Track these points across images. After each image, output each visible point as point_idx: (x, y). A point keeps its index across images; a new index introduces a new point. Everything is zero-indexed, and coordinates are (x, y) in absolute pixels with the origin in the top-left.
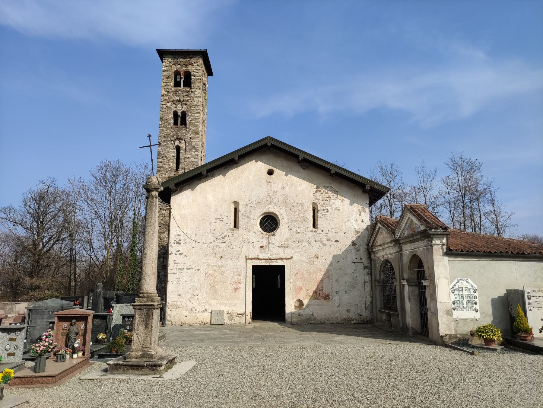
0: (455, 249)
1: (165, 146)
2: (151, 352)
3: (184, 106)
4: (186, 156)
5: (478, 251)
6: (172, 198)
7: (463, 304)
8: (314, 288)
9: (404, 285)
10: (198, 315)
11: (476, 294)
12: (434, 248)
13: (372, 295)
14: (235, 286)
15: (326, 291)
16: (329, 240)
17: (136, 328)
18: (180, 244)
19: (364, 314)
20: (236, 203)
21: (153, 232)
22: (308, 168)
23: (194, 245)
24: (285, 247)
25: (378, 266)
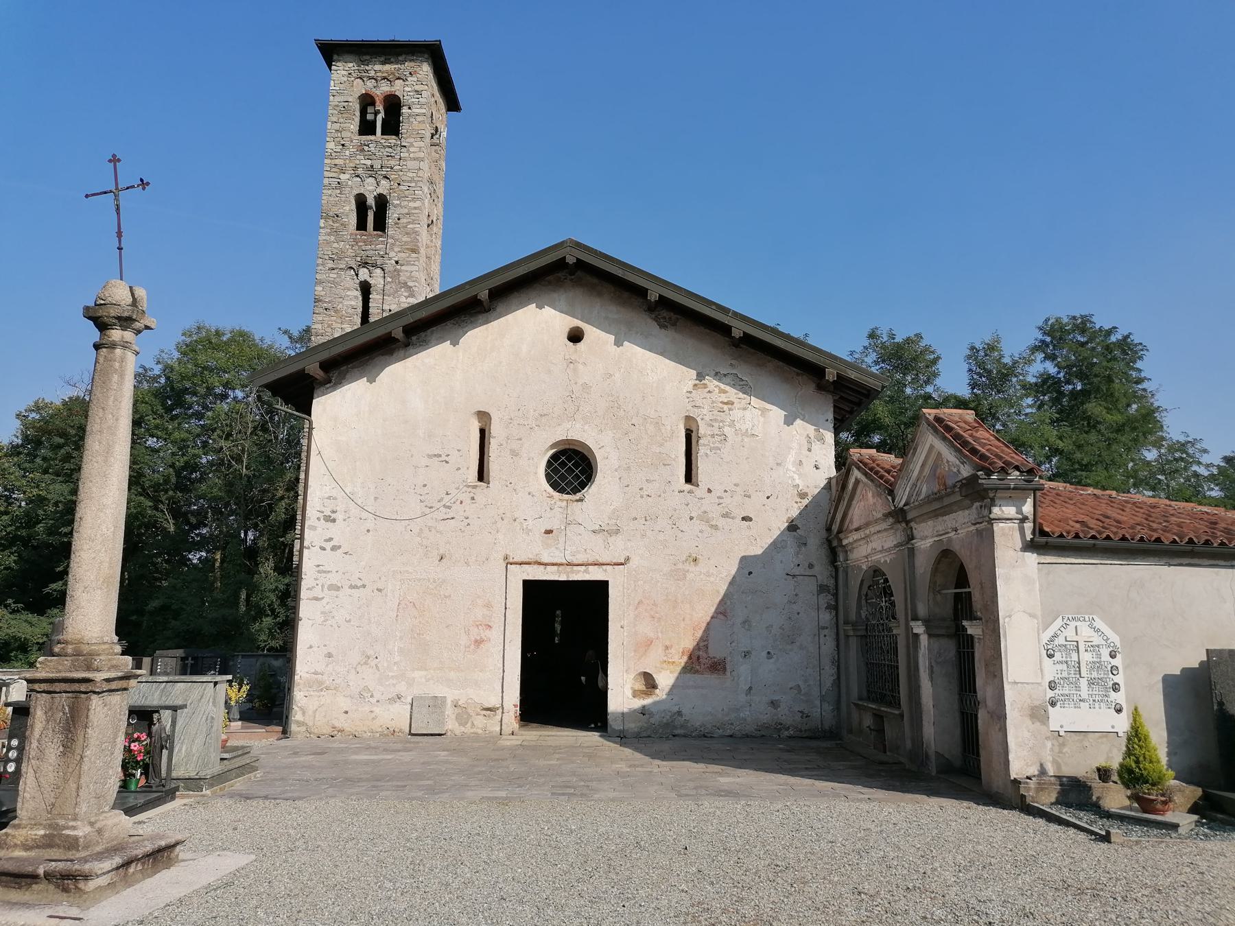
0: (1057, 532)
2: (74, 828)
3: (383, 182)
5: (1124, 539)
7: (1078, 688)
8: (689, 643)
9: (917, 636)
10: (377, 710)
11: (1117, 662)
12: (998, 527)
13: (838, 663)
14: (475, 633)
15: (716, 652)
16: (726, 515)
17: (33, 753)
18: (334, 521)
19: (816, 712)
20: (483, 416)
21: (108, 451)
22: (674, 325)
23: (370, 524)
25: (854, 584)
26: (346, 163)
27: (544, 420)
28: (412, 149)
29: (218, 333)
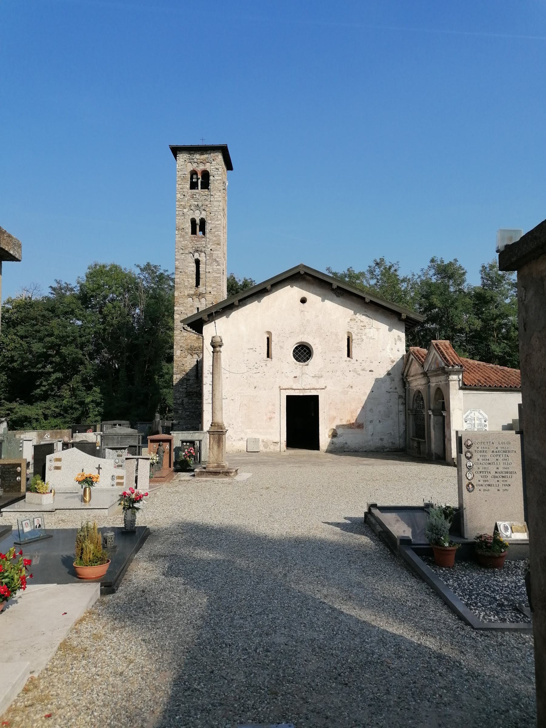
0: (469, 384)
1: (183, 260)
3: (203, 212)
4: (207, 271)
6: (204, 327)
9: (430, 415)
10: (234, 443)
12: (451, 383)
13: (406, 424)
16: (363, 370)
24: (319, 377)
26: (186, 204)
27: (292, 334)
28: (215, 196)
29: (104, 266)
